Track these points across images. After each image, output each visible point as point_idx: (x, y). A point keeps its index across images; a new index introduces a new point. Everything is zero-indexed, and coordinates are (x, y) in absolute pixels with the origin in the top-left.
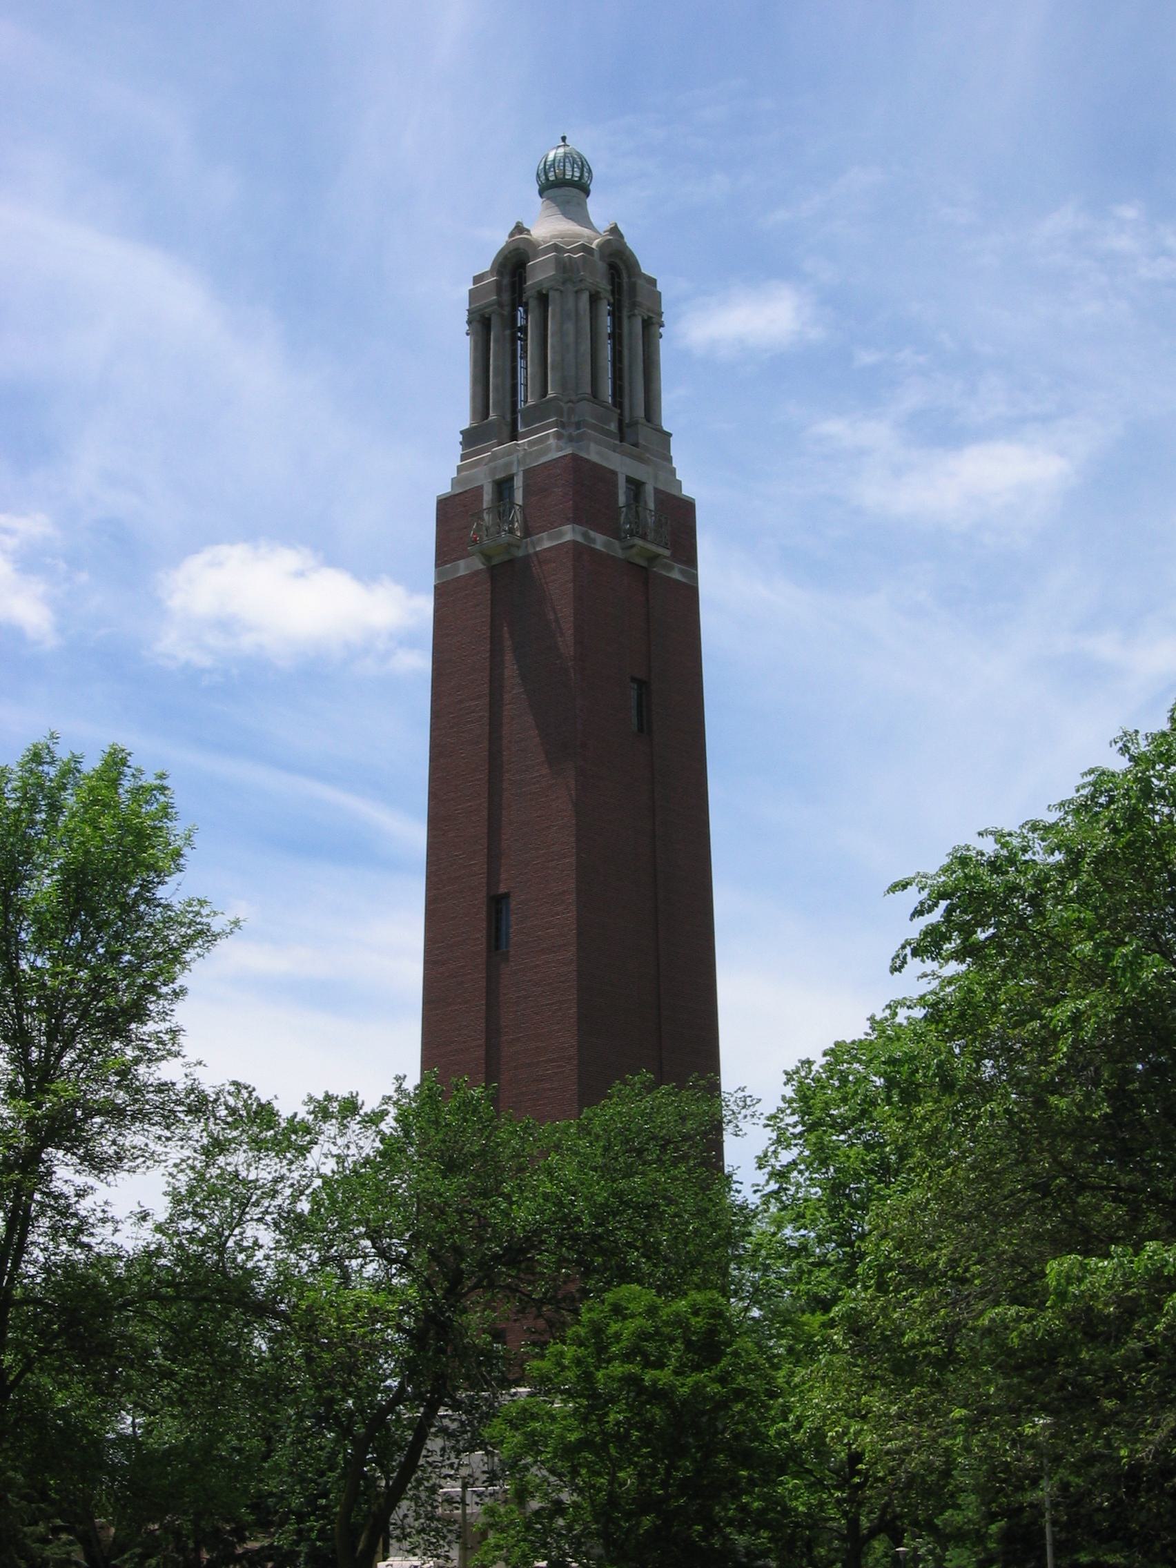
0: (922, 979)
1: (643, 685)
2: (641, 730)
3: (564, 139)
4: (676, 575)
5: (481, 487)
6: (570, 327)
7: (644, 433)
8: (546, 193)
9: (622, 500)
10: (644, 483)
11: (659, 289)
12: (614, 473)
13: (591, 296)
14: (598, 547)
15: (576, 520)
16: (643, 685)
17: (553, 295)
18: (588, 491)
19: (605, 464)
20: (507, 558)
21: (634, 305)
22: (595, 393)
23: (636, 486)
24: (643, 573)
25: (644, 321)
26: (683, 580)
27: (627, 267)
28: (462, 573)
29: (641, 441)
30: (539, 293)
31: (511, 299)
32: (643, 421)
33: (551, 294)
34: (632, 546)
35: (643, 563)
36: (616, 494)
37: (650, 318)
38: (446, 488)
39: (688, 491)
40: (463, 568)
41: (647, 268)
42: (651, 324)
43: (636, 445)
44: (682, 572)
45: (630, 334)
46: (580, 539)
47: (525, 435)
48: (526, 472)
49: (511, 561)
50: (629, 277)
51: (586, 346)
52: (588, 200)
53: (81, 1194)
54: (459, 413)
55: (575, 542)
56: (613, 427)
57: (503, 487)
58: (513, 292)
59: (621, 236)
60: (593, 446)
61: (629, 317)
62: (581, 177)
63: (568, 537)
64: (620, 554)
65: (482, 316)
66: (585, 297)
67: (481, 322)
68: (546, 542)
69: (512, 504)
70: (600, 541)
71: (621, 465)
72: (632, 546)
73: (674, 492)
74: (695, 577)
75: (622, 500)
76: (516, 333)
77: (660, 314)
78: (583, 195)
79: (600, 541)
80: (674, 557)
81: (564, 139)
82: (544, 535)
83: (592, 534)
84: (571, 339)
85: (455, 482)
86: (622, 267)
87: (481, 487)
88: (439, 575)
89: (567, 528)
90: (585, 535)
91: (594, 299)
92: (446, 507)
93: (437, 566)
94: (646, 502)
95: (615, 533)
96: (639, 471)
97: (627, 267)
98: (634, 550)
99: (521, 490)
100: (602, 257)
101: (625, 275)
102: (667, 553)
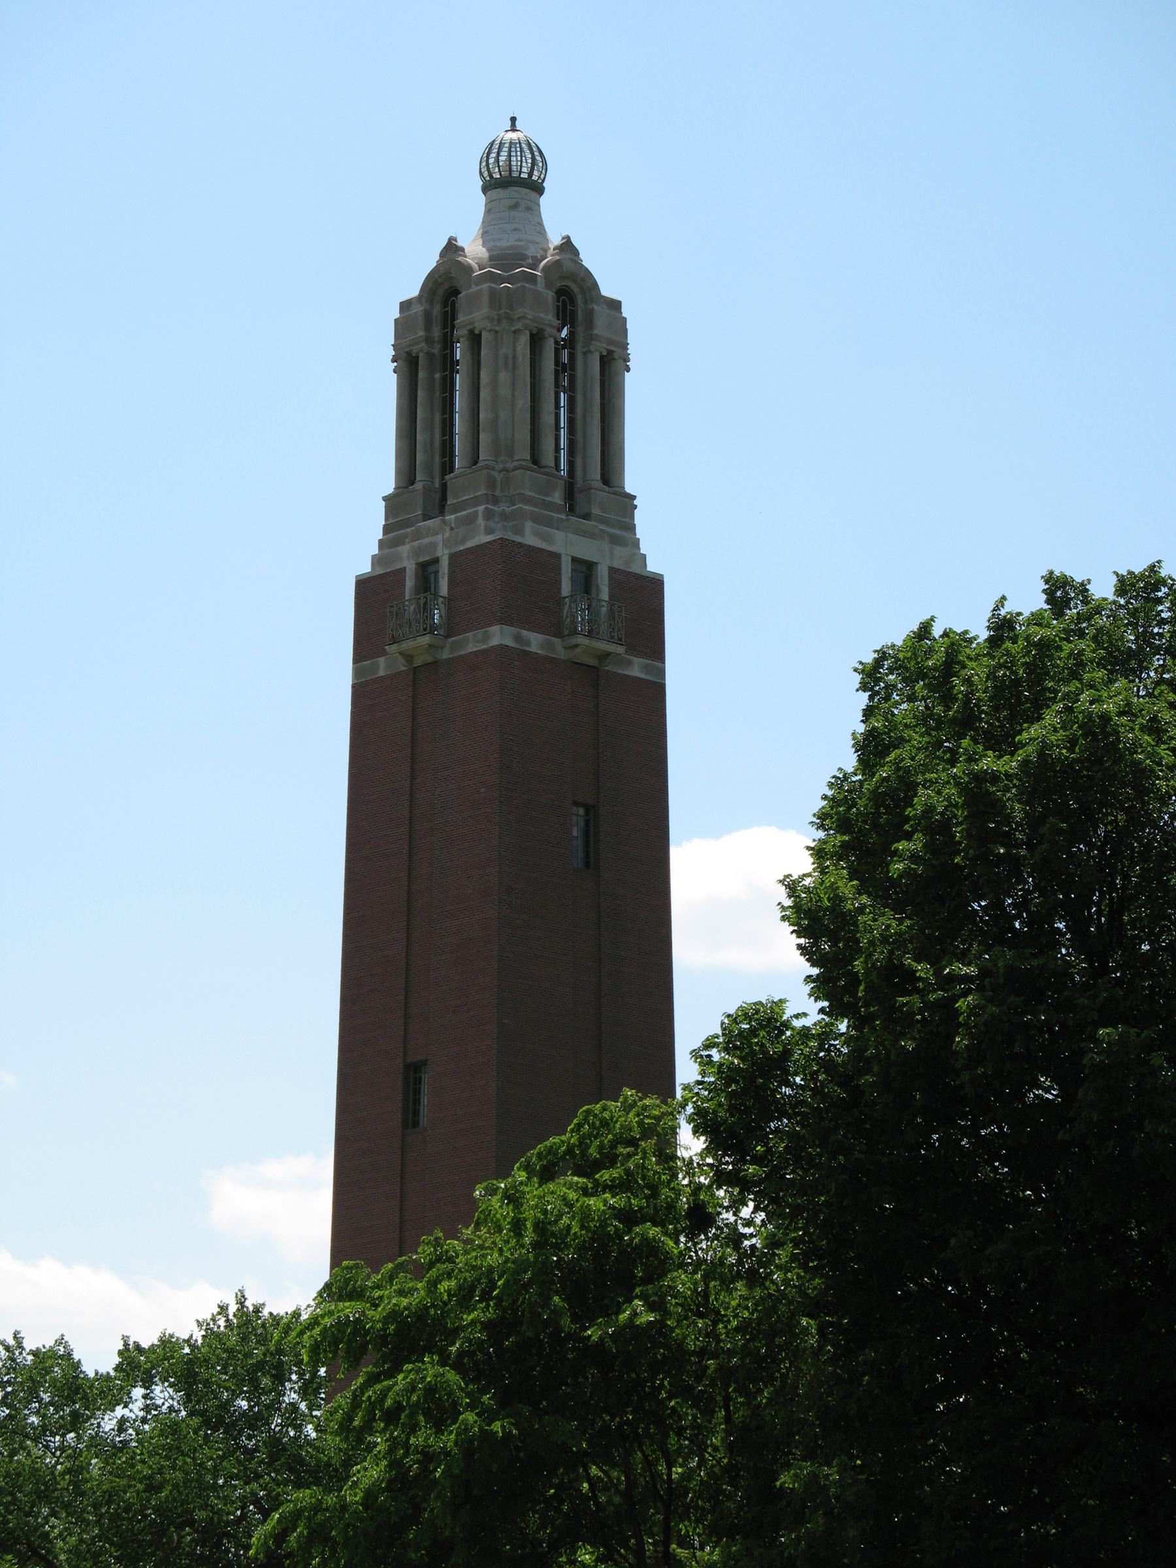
0: (92, 1375)
1: (591, 810)
2: (587, 865)
3: (513, 120)
5: (404, 569)
6: (503, 376)
7: (601, 495)
9: (566, 589)
10: (596, 563)
12: (557, 556)
13: (532, 336)
14: (534, 649)
15: (505, 621)
17: (485, 336)
18: (520, 582)
20: (429, 659)
21: (591, 338)
22: (535, 460)
23: (585, 570)
24: (592, 675)
25: (602, 357)
26: (647, 677)
27: (583, 291)
28: (382, 672)
29: (596, 511)
30: (471, 332)
31: (441, 333)
32: (600, 485)
35: (593, 662)
36: (558, 582)
37: (610, 352)
38: (366, 568)
39: (653, 566)
40: (382, 667)
41: (607, 290)
43: (587, 516)
44: (647, 669)
45: (585, 373)
46: (510, 642)
47: (456, 509)
48: (453, 557)
49: (435, 662)
50: (586, 303)
51: (523, 401)
52: (544, 200)
54: (381, 474)
55: (502, 647)
56: (557, 497)
57: (426, 570)
58: (445, 326)
59: (576, 252)
60: (529, 525)
61: (585, 354)
62: (531, 174)
63: (495, 641)
64: (561, 653)
65: (409, 354)
66: (524, 340)
67: (408, 363)
68: (471, 644)
69: (436, 595)
70: (536, 642)
71: (567, 544)
72: (576, 646)
73: (635, 568)
74: (662, 673)
75: (566, 589)
76: (449, 365)
77: (625, 346)
78: (534, 194)
79: (536, 642)
80: (633, 649)
81: (513, 120)
82: (470, 635)
83: (524, 633)
85: (376, 561)
86: (576, 290)
87: (404, 569)
88: (357, 673)
89: (495, 629)
90: (518, 638)
92: (364, 587)
93: (356, 660)
94: (598, 590)
95: (556, 628)
96: (586, 549)
97: (583, 291)
98: (578, 650)
100: (549, 284)
101: (579, 298)
102: (621, 650)
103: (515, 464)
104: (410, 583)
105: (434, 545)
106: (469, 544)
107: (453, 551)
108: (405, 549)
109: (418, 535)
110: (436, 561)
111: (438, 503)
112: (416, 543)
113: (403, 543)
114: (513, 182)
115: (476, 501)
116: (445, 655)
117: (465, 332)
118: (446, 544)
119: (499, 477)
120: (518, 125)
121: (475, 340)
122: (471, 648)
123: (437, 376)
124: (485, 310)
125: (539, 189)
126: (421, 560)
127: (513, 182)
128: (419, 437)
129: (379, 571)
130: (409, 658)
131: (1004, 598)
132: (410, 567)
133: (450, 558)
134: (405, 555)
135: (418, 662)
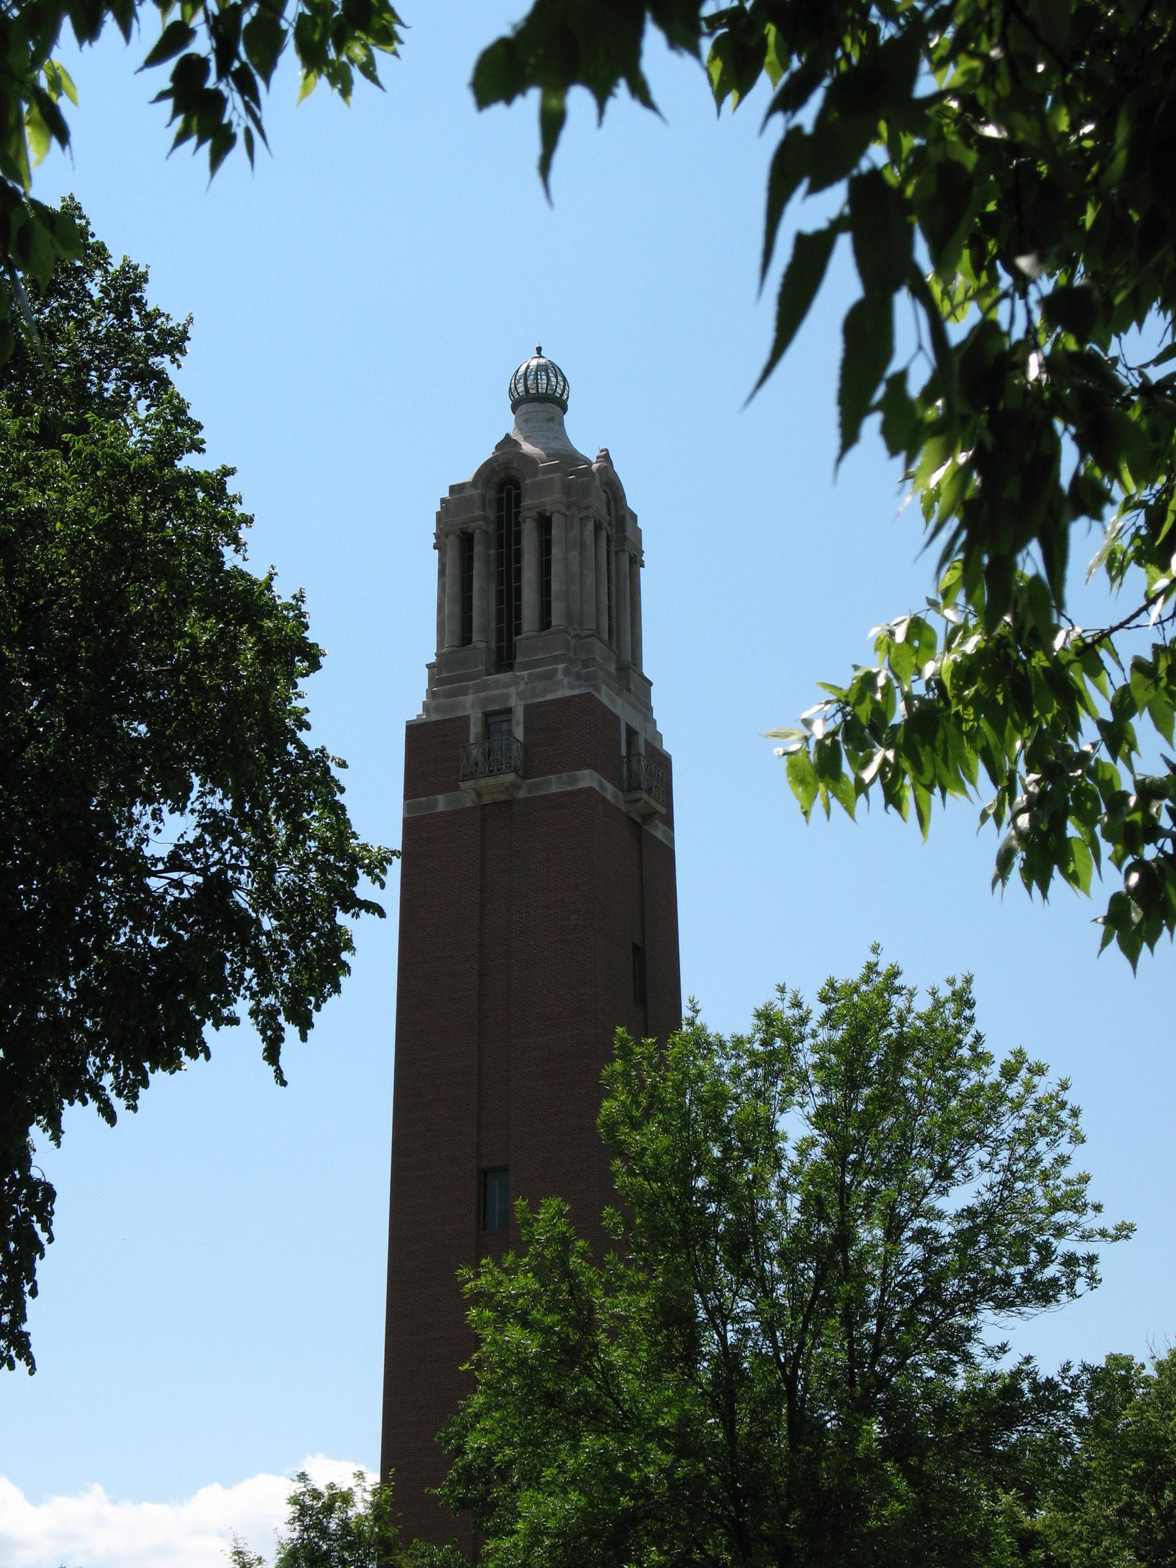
1: (638, 950)
3: (539, 350)
4: (659, 835)
6: (574, 555)
8: (523, 408)
11: (639, 525)
12: (618, 718)
14: (609, 797)
16: (638, 950)
19: (611, 707)
23: (632, 733)
25: (630, 557)
28: (441, 808)
29: (632, 688)
33: (555, 517)
34: (637, 801)
35: (638, 819)
39: (667, 746)
40: (442, 803)
42: (636, 561)
45: (617, 568)
46: (596, 786)
47: (526, 666)
52: (567, 418)
53: (365, 1501)
57: (497, 718)
58: (500, 509)
61: (617, 553)
62: (562, 395)
63: (584, 784)
64: (623, 807)
66: (590, 526)
72: (637, 801)
81: (539, 350)
82: (554, 777)
84: (576, 569)
87: (468, 718)
88: (408, 808)
89: (586, 772)
91: (598, 528)
92: (414, 732)
93: (407, 796)
99: (521, 727)
103: (585, 633)
104: (475, 729)
105: (507, 697)
106: (549, 697)
107: (530, 702)
108: (469, 699)
109: (485, 687)
110: (509, 711)
111: (504, 660)
112: (483, 695)
113: (466, 694)
114: (541, 398)
115: (555, 660)
116: (522, 794)
117: (533, 513)
118: (520, 695)
119: (572, 642)
120: (543, 354)
121: (544, 523)
122: (554, 789)
123: (492, 552)
124: (557, 496)
125: (564, 409)
126: (489, 708)
127: (541, 398)
128: (476, 603)
129: (435, 717)
130: (479, 795)
131: (1162, 755)
132: (476, 717)
133: (525, 709)
134: (468, 704)
135: (487, 800)
